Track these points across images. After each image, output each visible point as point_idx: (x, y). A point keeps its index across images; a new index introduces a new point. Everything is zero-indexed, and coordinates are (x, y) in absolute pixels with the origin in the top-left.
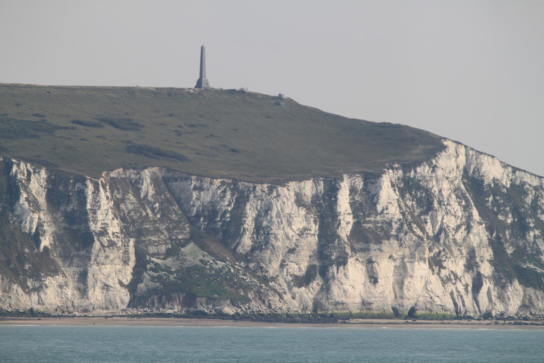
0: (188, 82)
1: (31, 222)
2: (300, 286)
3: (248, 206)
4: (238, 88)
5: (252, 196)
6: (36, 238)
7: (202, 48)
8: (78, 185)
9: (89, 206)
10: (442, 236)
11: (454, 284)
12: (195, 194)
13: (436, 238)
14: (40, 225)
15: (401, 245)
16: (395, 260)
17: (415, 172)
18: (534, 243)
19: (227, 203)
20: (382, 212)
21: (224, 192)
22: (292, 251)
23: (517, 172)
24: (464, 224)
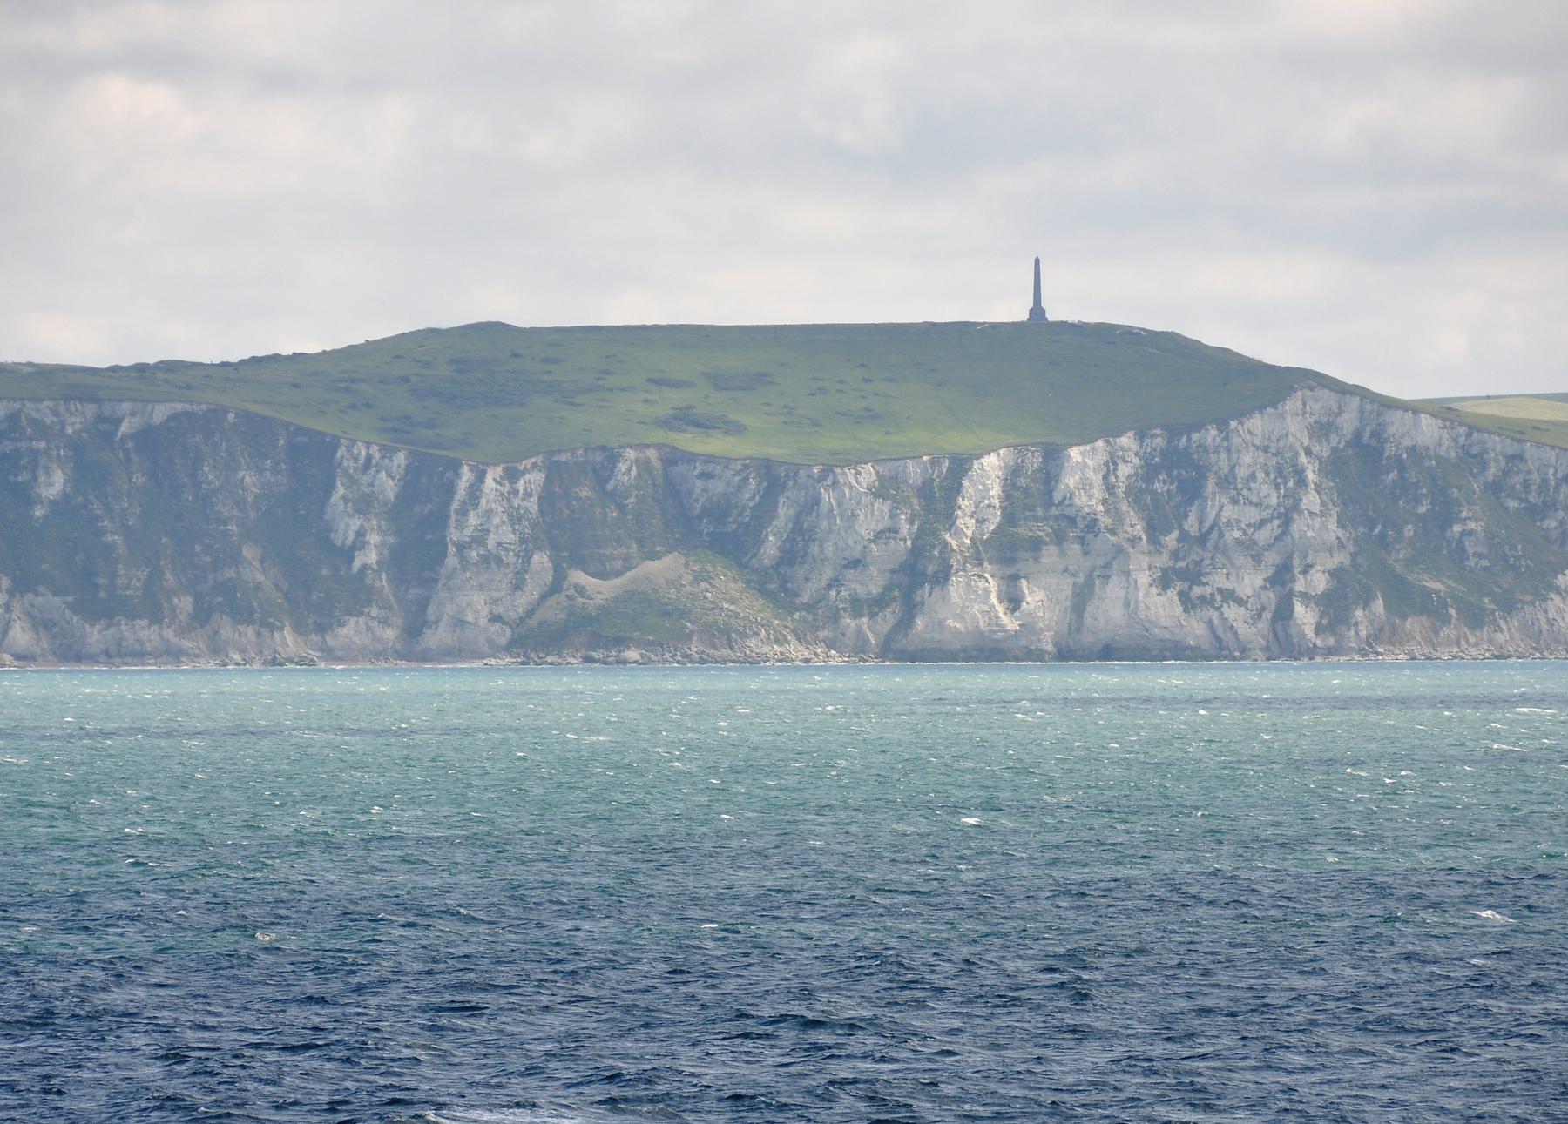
0: (1015, 311)
1: (346, 531)
2: (857, 615)
3: (782, 499)
4: (247, 357)
5: (791, 484)
6: (348, 554)
7: (1037, 262)
8: (449, 474)
9: (455, 505)
10: (1214, 535)
11: (1218, 609)
12: (699, 484)
13: (1202, 540)
14: (361, 533)
15: (1086, 553)
16: (1074, 575)
17: (1189, 440)
18: (1460, 542)
19: (747, 496)
20: (1061, 503)
21: (746, 479)
22: (855, 563)
23: (1475, 434)
24: (1279, 517)
